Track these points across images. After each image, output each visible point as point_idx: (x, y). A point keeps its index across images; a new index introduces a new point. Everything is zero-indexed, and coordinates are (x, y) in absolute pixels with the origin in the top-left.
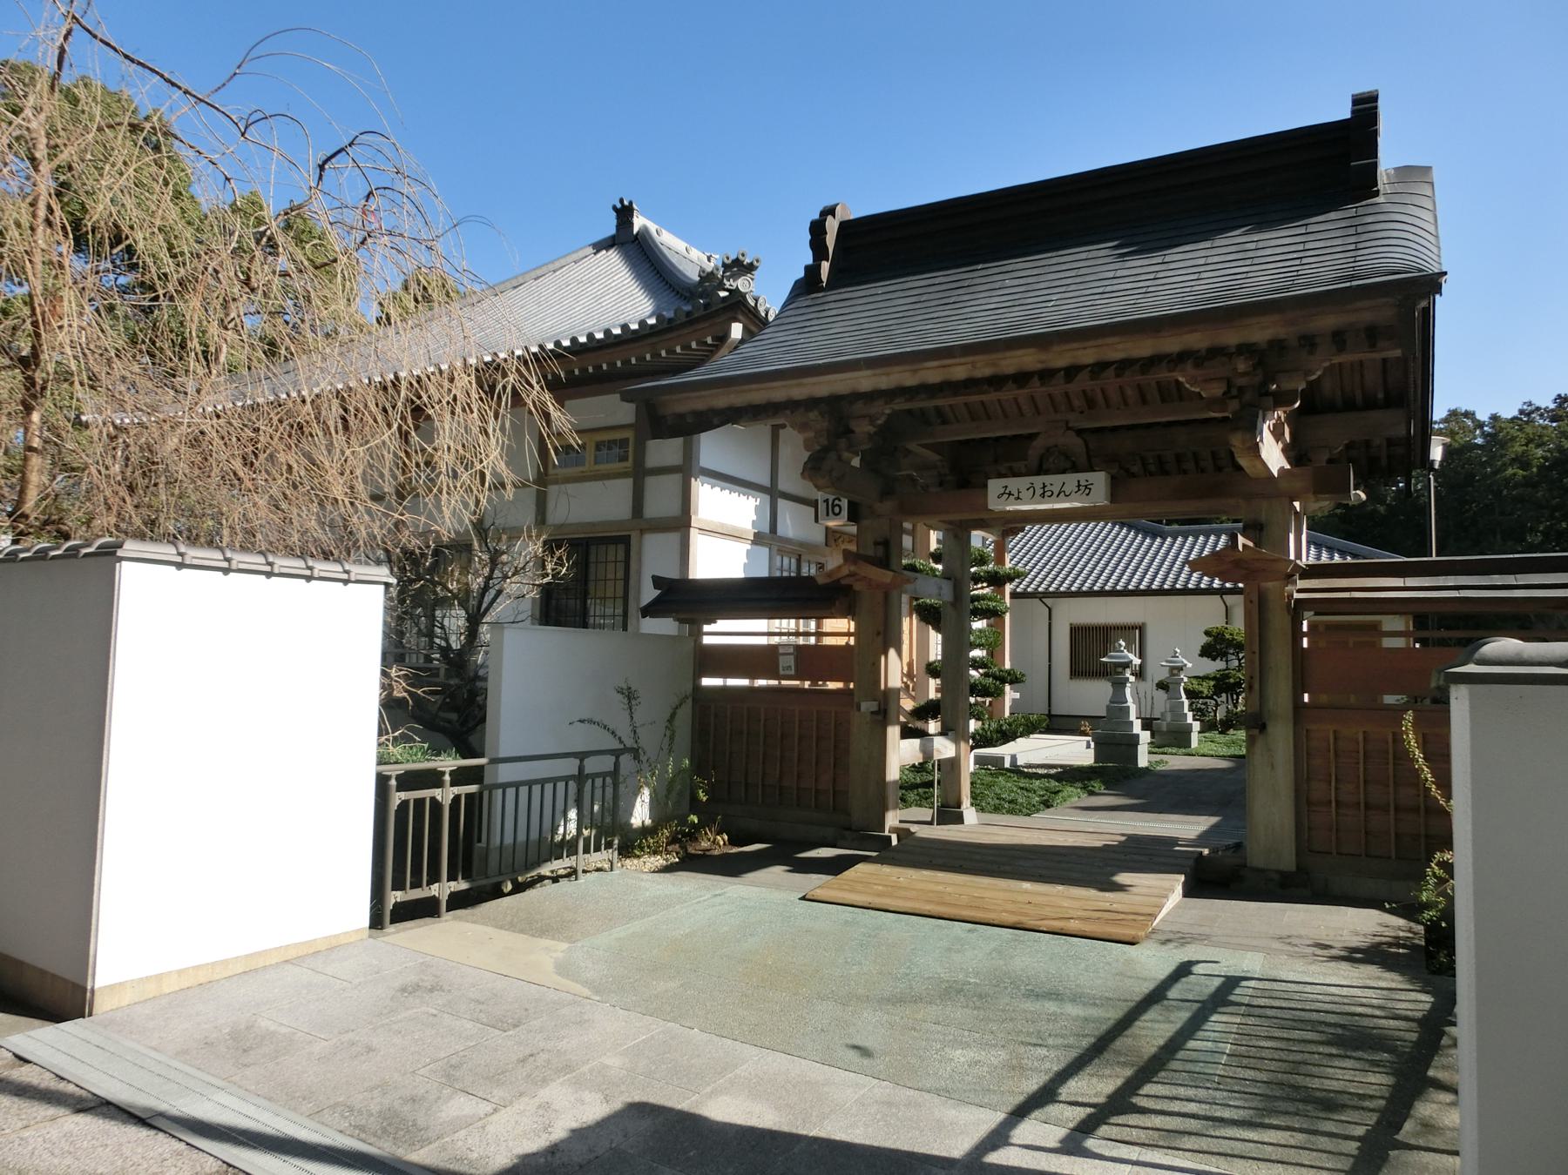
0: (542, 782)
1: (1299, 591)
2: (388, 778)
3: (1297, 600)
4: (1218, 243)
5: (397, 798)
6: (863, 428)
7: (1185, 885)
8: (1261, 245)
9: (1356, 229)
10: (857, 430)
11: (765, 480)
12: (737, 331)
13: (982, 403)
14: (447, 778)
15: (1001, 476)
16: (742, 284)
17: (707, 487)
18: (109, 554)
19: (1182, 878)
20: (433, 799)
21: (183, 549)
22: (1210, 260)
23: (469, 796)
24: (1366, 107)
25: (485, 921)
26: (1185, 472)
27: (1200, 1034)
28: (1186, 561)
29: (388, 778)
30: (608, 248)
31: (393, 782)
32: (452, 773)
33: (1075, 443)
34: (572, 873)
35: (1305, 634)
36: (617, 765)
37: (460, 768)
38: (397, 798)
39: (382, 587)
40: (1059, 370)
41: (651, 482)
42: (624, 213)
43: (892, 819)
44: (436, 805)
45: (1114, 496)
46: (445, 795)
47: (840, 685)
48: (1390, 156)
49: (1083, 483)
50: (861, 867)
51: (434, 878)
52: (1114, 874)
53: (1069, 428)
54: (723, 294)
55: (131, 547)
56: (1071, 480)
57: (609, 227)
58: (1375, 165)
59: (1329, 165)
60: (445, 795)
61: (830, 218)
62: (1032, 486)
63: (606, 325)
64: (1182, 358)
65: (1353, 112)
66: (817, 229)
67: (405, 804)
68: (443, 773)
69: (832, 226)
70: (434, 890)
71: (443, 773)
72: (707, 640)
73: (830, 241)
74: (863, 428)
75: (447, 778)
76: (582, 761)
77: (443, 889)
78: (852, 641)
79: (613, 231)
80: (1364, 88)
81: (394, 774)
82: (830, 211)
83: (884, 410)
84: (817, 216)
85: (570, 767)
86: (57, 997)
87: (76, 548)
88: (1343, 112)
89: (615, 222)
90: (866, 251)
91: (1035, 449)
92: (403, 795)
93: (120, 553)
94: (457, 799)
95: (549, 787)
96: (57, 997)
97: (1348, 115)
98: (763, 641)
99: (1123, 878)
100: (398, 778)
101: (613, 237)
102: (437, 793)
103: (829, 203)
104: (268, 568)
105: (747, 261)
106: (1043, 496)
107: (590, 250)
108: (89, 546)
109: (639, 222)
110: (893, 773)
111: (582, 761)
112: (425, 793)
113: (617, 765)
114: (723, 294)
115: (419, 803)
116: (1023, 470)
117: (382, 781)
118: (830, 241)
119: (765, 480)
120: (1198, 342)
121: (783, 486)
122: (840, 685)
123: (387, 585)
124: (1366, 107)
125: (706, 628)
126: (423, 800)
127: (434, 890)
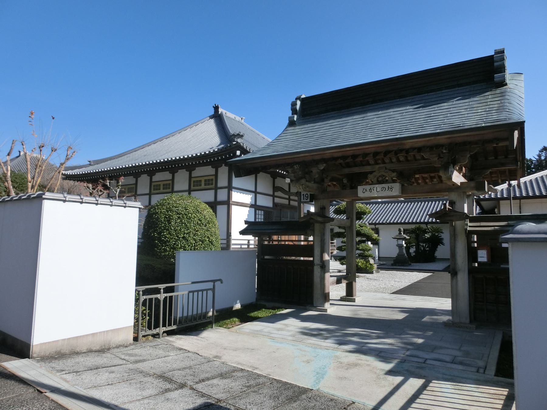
0: (198, 291)
1: (470, 226)
2: (139, 292)
5: (142, 298)
11: (253, 190)
12: (238, 153)
14: (162, 291)
16: (239, 140)
17: (236, 193)
18: (40, 198)
20: (157, 299)
21: (66, 195)
28: (427, 215)
29: (139, 292)
30: (212, 118)
31: (141, 293)
32: (143, 291)
35: (475, 242)
36: (214, 286)
37: (167, 287)
39: (138, 209)
40: (360, 155)
41: (219, 191)
42: (216, 108)
46: (161, 296)
54: (234, 143)
55: (48, 195)
57: (212, 112)
59: (485, 74)
63: (201, 152)
67: (145, 300)
68: (160, 289)
71: (160, 289)
75: (162, 291)
76: (214, 283)
77: (162, 329)
79: (213, 113)
80: (499, 47)
81: (141, 290)
85: (210, 285)
86: (21, 350)
87: (29, 196)
89: (214, 111)
92: (145, 297)
93: (44, 197)
95: (200, 293)
96: (21, 350)
100: (164, 289)
101: (213, 115)
102: (158, 296)
105: (241, 134)
107: (209, 118)
108: (34, 194)
109: (220, 110)
111: (214, 283)
112: (153, 296)
113: (214, 286)
114: (234, 143)
115: (151, 300)
116: (375, 180)
117: (137, 292)
119: (254, 190)
121: (258, 190)
123: (140, 208)
126: (152, 298)
127: (157, 331)
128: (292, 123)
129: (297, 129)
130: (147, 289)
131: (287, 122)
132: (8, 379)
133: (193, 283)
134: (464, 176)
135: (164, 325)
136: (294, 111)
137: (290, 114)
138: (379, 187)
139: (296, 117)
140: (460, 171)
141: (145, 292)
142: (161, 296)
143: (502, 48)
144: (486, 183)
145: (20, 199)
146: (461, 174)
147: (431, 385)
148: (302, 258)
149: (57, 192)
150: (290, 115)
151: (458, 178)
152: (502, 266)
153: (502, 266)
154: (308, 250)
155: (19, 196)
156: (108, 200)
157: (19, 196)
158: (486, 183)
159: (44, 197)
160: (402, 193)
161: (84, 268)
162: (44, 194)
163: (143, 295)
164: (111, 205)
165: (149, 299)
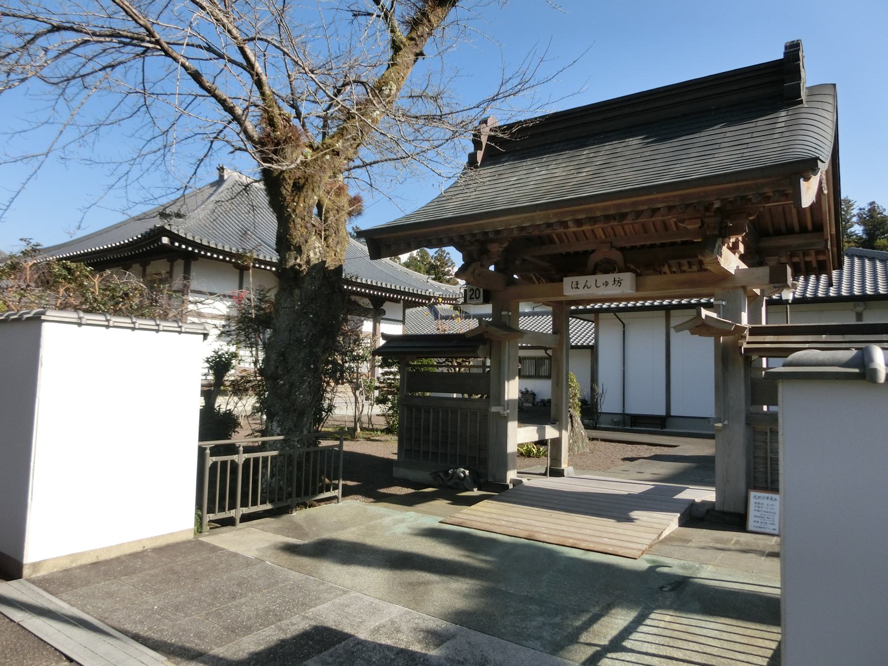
1: (748, 343)
2: (205, 449)
4: (703, 134)
5: (210, 460)
7: (680, 519)
8: (749, 136)
9: (793, 125)
13: (583, 231)
14: (241, 449)
18: (37, 320)
19: (679, 515)
20: (233, 462)
21: (109, 317)
23: (273, 457)
24: (793, 51)
26: (684, 272)
27: (648, 622)
29: (205, 449)
31: (208, 451)
32: (211, 449)
33: (617, 256)
38: (210, 460)
43: (512, 475)
45: (638, 288)
47: (460, 396)
48: (810, 77)
50: (484, 503)
51: (233, 506)
52: (632, 510)
53: (613, 247)
55: (51, 314)
56: (609, 277)
59: (773, 86)
65: (785, 53)
67: (215, 464)
70: (232, 513)
73: (484, 140)
74: (495, 248)
77: (239, 511)
78: (213, 388)
81: (208, 447)
88: (779, 55)
92: (214, 459)
93: (43, 317)
94: (247, 461)
97: (781, 57)
99: (635, 514)
100: (211, 449)
102: (235, 457)
104: (179, 329)
110: (512, 448)
115: (224, 463)
117: (201, 451)
120: (685, 193)
122: (460, 396)
124: (793, 51)
127: (232, 513)
128: (472, 161)
129: (487, 172)
130: (216, 446)
133: (624, 459)
134: (742, 258)
135: (244, 504)
136: (477, 144)
137: (471, 148)
138: (601, 278)
140: (734, 248)
141: (215, 451)
143: (795, 39)
144: (789, 270)
146: (737, 255)
147: (652, 616)
151: (730, 261)
158: (789, 270)
159: (43, 317)
160: (637, 289)
162: (44, 313)
163: (211, 455)
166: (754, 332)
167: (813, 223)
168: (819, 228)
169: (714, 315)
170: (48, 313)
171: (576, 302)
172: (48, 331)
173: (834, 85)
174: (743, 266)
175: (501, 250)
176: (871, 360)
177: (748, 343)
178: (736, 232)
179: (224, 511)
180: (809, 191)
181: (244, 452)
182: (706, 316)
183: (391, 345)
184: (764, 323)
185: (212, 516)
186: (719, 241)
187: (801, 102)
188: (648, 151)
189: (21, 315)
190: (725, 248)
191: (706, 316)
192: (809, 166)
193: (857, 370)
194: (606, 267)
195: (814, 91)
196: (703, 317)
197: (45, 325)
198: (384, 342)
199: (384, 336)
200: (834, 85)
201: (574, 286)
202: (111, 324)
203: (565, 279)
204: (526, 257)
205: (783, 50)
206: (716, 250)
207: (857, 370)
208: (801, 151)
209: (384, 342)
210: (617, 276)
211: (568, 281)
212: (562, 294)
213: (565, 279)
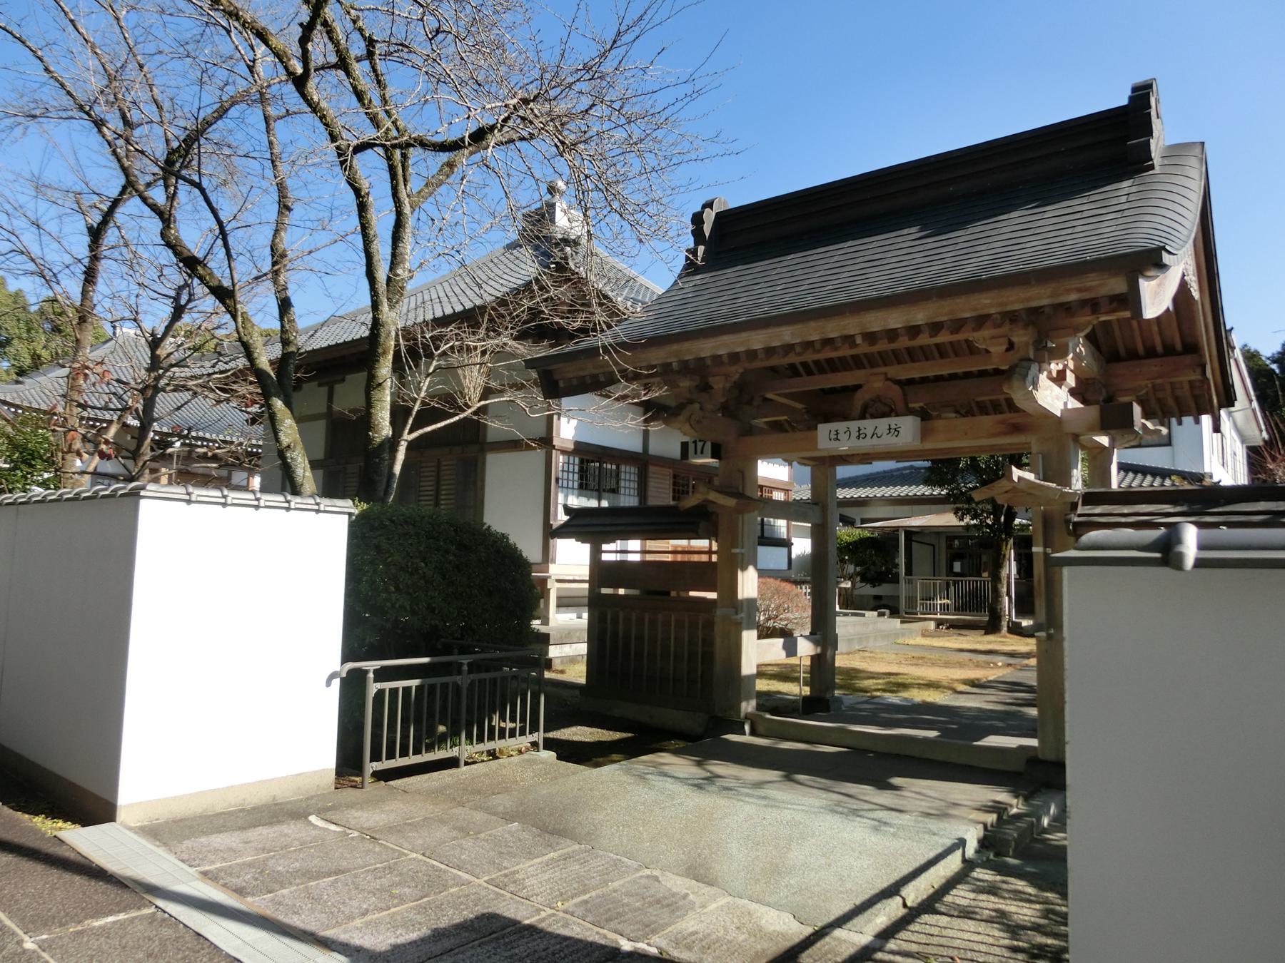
1: (1080, 515)
3: (1075, 524)
6: (718, 384)
10: (715, 386)
13: (967, 341)
15: (827, 419)
18: (135, 495)
22: (1119, 215)
24: (1142, 94)
25: (628, 772)
27: (911, 927)
31: (371, 675)
32: (375, 672)
34: (452, 763)
38: (373, 688)
39: (346, 517)
44: (457, 688)
49: (893, 426)
52: (892, 777)
56: (883, 423)
58: (1147, 145)
59: (1111, 145)
60: (463, 680)
61: (708, 210)
62: (849, 431)
64: (981, 321)
65: (1131, 98)
66: (697, 219)
67: (380, 693)
69: (709, 217)
71: (367, 672)
72: (605, 557)
73: (707, 229)
80: (1140, 79)
81: (372, 669)
82: (709, 205)
83: (736, 371)
84: (699, 209)
90: (735, 237)
91: (860, 398)
92: (379, 685)
93: (142, 493)
97: (1125, 102)
98: (669, 558)
99: (896, 781)
100: (375, 672)
102: (458, 679)
103: (710, 198)
106: (858, 437)
115: (394, 692)
118: (707, 229)
123: (350, 514)
124: (1142, 94)
125: (605, 547)
126: (396, 690)
130: (383, 668)
131: (681, 262)
132: (24, 855)
134: (1073, 392)
136: (698, 234)
139: (701, 249)
140: (1059, 379)
142: (463, 680)
145: (94, 497)
146: (1065, 389)
148: (621, 591)
149: (170, 483)
150: (691, 244)
151: (1053, 396)
152: (692, 594)
153: (692, 594)
154: (703, 574)
155: (60, 492)
156: (181, 490)
157: (60, 492)
161: (231, 636)
164: (189, 502)
165: (442, 684)
166: (1089, 499)
167: (1183, 342)
168: (1192, 348)
169: (1030, 476)
170: (148, 487)
171: (845, 459)
172: (147, 509)
173: (1203, 144)
174: (1074, 404)
175: (728, 385)
176: (1179, 541)
177: (1080, 515)
178: (1061, 354)
179: (407, 755)
180: (1156, 298)
181: (470, 672)
182: (1019, 478)
183: (574, 522)
184: (1114, 486)
185: (377, 766)
186: (1034, 367)
187: (1152, 167)
188: (931, 242)
189: (96, 492)
190: (1043, 377)
191: (1019, 478)
192: (1152, 260)
193: (1158, 555)
194: (879, 409)
195: (1177, 152)
196: (1015, 479)
197: (143, 502)
198: (566, 518)
199: (568, 510)
200: (1203, 144)
201: (833, 437)
202: (194, 498)
203: (820, 426)
204: (769, 396)
205: (1129, 93)
206: (1030, 378)
207: (1158, 555)
208: (1141, 239)
209: (566, 518)
210: (893, 421)
211: (824, 430)
212: (817, 449)
213: (820, 426)
